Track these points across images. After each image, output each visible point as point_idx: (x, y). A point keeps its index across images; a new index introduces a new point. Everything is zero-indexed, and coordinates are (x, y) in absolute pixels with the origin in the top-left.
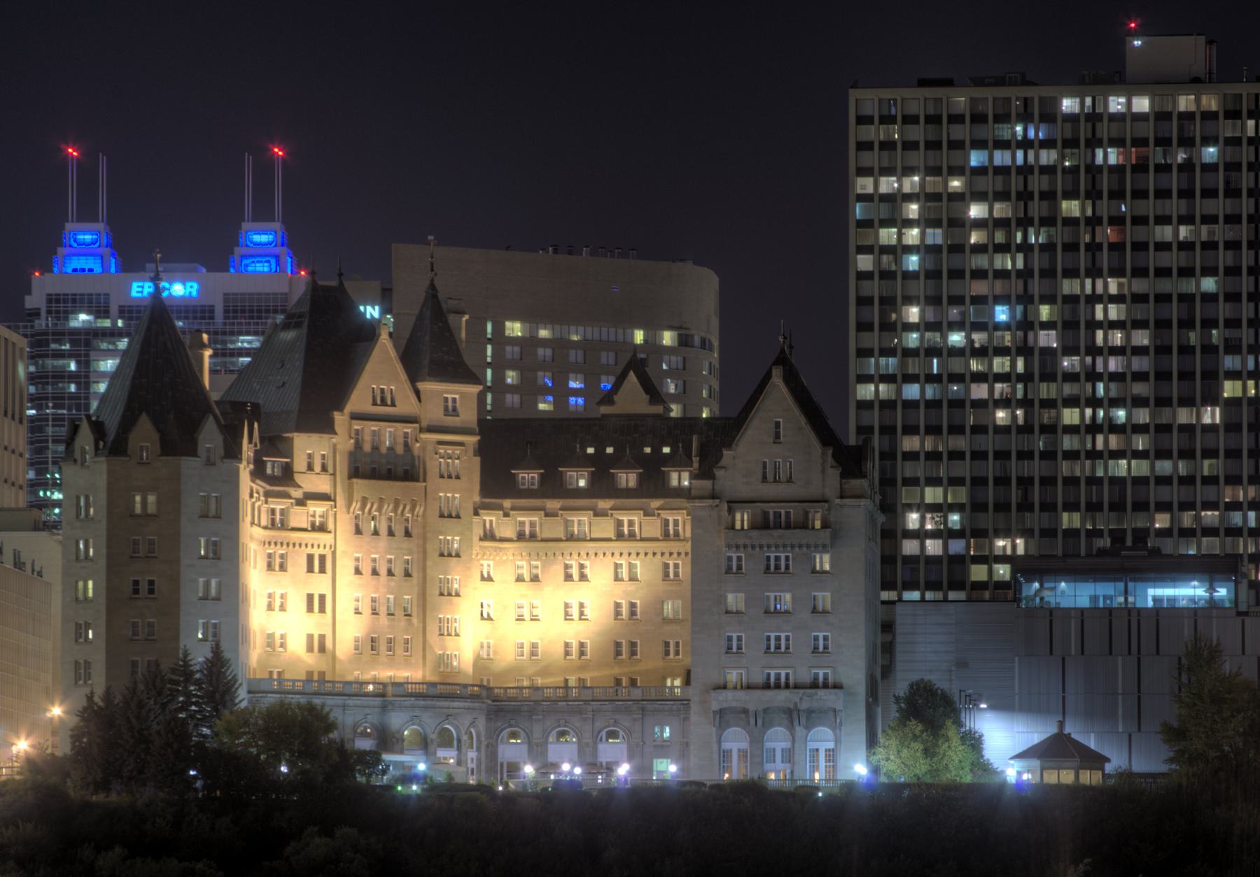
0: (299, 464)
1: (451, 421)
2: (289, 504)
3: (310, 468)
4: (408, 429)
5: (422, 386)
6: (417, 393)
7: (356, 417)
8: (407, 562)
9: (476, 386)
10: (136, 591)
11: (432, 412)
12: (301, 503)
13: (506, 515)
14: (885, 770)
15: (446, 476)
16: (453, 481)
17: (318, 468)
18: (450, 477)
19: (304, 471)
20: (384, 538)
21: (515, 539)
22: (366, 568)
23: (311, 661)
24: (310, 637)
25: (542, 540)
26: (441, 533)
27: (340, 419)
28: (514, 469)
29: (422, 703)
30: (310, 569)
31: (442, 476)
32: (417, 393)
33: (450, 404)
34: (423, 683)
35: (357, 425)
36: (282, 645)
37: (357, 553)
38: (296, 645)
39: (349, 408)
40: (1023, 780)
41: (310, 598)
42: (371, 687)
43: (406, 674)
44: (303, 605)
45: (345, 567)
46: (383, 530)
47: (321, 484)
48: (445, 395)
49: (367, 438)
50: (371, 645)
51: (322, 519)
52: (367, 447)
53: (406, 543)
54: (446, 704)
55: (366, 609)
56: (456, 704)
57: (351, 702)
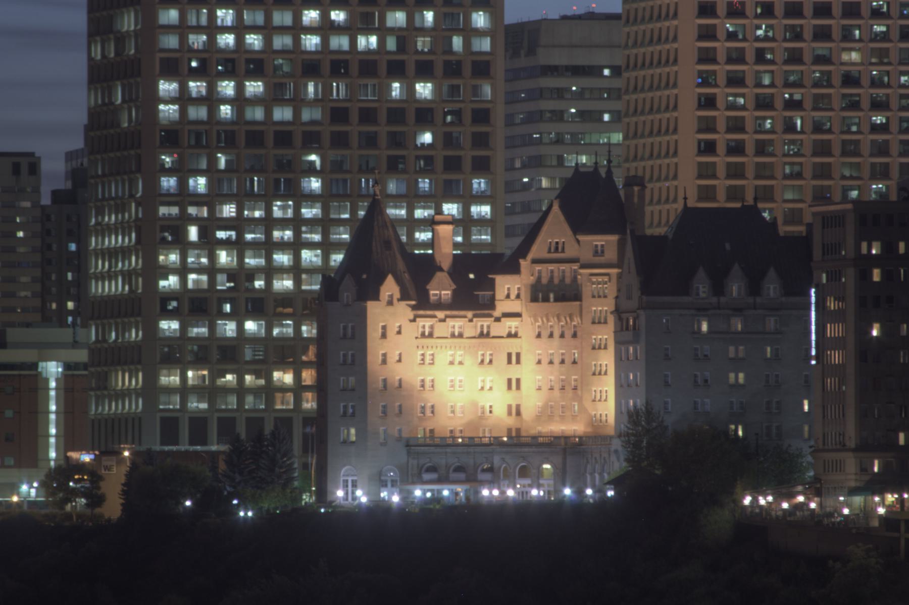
0: (500, 293)
1: (598, 260)
2: (435, 322)
3: (508, 296)
4: (575, 267)
5: (578, 237)
6: (578, 241)
7: (535, 261)
8: (563, 354)
9: (613, 236)
10: (452, 386)
11: (587, 255)
12: (498, 320)
13: (471, 321)
14: (398, 484)
15: (597, 296)
16: (602, 300)
17: (513, 296)
18: (599, 297)
19: (502, 298)
20: (556, 339)
21: (449, 337)
22: (545, 361)
23: (511, 422)
24: (510, 407)
25: (467, 338)
26: (593, 334)
27: (524, 264)
28: (476, 291)
29: (504, 450)
30: (509, 361)
31: (594, 297)
32: (578, 241)
33: (599, 248)
34: (551, 437)
35: (538, 268)
36: (491, 412)
37: (561, 349)
38: (500, 411)
39: (530, 256)
40: (13, 501)
41: (509, 381)
42: (460, 440)
43: (563, 428)
44: (523, 385)
45: (528, 361)
46: (557, 333)
47: (514, 306)
48: (595, 243)
49: (568, 274)
50: (546, 413)
51: (460, 330)
52: (556, 281)
53: (573, 342)
54: (518, 449)
55: (545, 388)
56: (526, 449)
57: (449, 450)
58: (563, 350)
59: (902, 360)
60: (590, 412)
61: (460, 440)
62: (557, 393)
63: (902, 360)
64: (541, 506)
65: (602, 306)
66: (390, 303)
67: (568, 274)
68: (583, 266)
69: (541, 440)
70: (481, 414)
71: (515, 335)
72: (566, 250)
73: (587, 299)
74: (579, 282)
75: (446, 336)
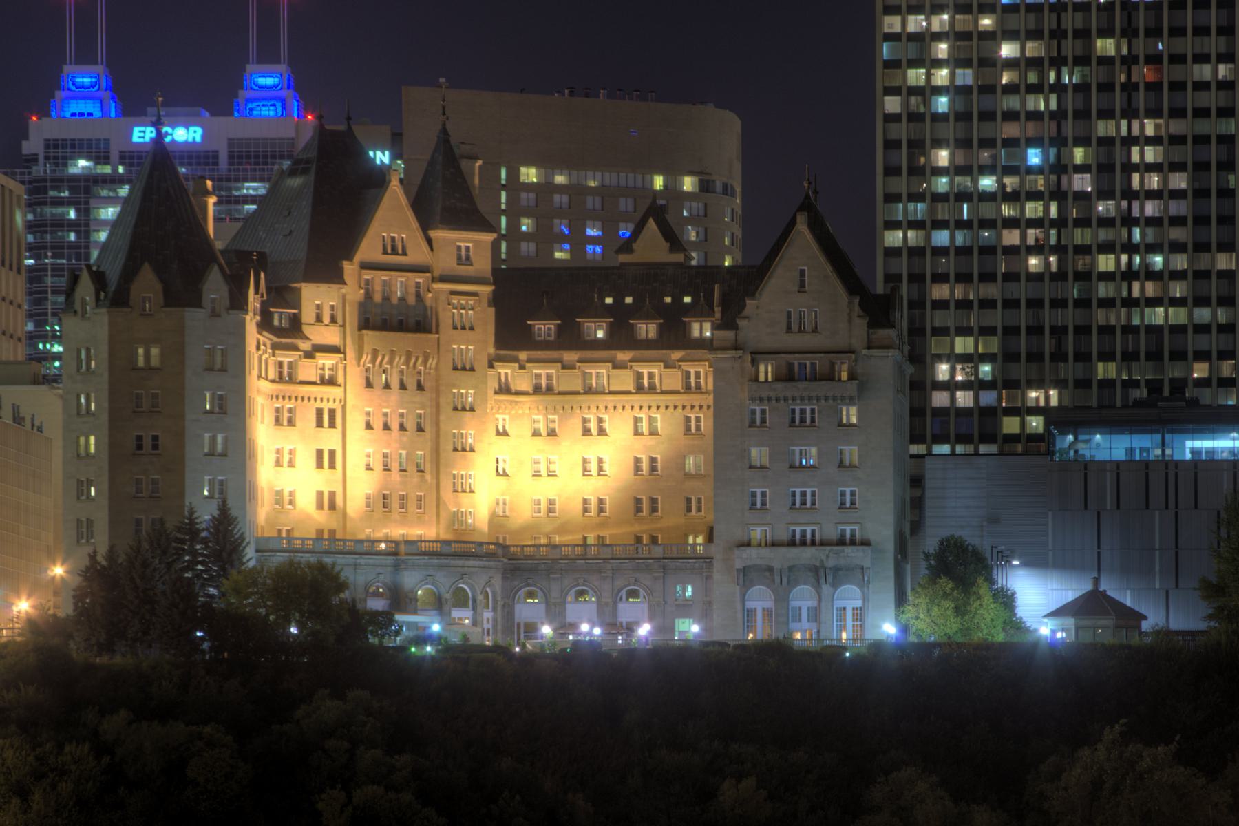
2: (297, 357)
3: (319, 319)
4: (420, 278)
6: (429, 241)
7: (365, 266)
8: (420, 416)
11: (445, 262)
12: (309, 355)
16: (468, 332)
17: (326, 319)
19: (312, 322)
22: (377, 423)
23: (321, 519)
26: (455, 386)
27: (349, 268)
30: (320, 424)
31: (455, 328)
32: (429, 241)
33: (463, 253)
34: (436, 542)
35: (367, 275)
36: (291, 503)
38: (306, 503)
41: (320, 453)
43: (419, 532)
45: (355, 422)
46: (395, 383)
47: (330, 336)
48: (458, 244)
49: (378, 288)
52: (378, 298)
54: (460, 562)
56: (471, 563)
57: (363, 560)
58: (403, 409)
59: (92, 439)
60: (450, 507)
61: (383, 546)
62: (395, 476)
63: (92, 439)
64: (589, 654)
65: (467, 343)
66: (215, 314)
67: (378, 288)
68: (444, 279)
69: (423, 547)
70: (801, 504)
71: (332, 382)
72: (408, 252)
73: (446, 331)
74: (428, 303)
75: (313, 379)
